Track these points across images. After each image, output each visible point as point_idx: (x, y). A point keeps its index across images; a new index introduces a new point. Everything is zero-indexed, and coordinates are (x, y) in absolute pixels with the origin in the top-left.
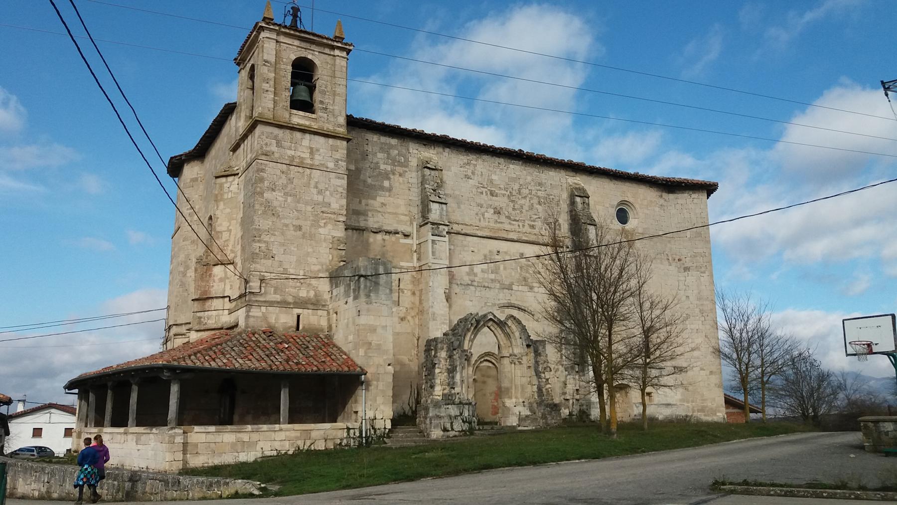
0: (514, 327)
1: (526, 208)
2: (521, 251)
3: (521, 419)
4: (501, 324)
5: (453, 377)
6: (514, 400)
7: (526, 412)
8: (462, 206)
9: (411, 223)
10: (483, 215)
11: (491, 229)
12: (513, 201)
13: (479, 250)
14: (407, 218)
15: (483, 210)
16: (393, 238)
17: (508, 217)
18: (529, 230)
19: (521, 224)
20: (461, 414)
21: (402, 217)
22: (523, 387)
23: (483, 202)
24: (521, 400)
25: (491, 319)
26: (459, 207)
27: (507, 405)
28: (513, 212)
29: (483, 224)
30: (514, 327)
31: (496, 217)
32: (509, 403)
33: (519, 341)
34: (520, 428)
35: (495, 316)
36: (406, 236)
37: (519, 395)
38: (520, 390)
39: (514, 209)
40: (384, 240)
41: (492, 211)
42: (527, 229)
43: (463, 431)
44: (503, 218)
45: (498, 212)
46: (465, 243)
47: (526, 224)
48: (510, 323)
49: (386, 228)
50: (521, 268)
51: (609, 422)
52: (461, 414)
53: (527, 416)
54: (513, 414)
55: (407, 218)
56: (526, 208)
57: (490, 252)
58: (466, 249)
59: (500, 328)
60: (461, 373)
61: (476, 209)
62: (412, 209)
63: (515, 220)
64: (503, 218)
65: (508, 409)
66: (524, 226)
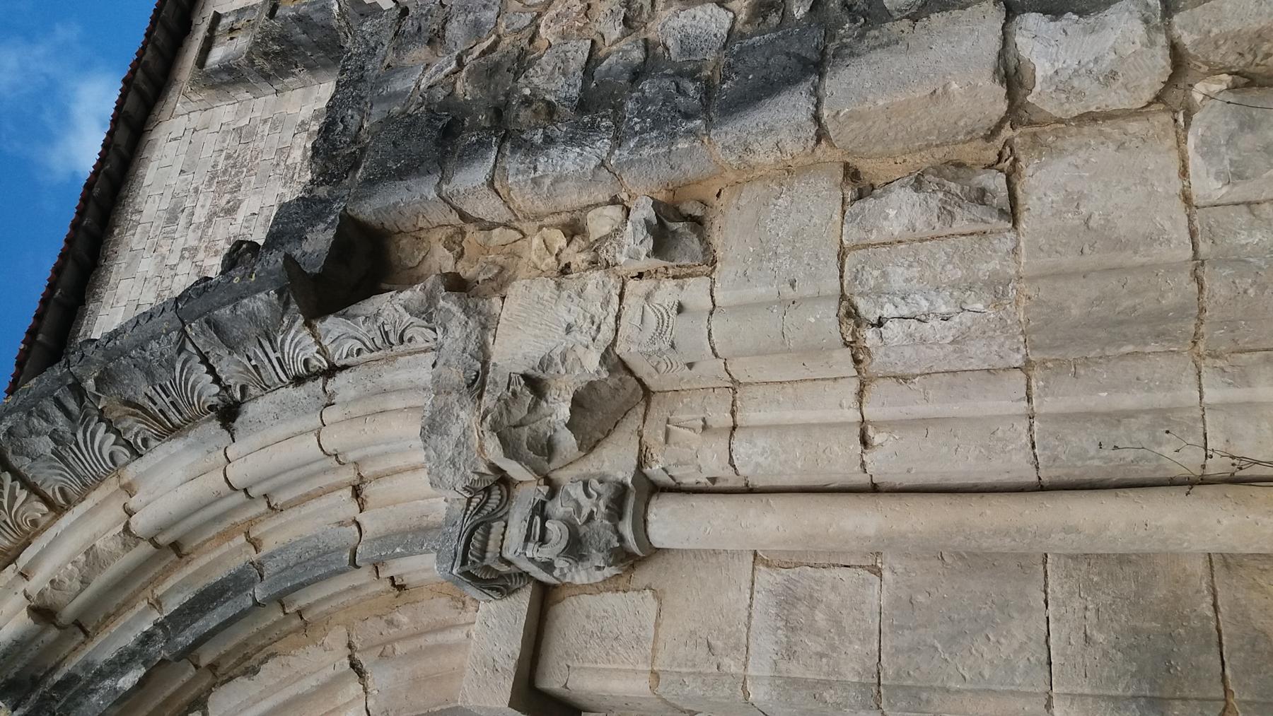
33: (276, 439)
38: (1157, 383)
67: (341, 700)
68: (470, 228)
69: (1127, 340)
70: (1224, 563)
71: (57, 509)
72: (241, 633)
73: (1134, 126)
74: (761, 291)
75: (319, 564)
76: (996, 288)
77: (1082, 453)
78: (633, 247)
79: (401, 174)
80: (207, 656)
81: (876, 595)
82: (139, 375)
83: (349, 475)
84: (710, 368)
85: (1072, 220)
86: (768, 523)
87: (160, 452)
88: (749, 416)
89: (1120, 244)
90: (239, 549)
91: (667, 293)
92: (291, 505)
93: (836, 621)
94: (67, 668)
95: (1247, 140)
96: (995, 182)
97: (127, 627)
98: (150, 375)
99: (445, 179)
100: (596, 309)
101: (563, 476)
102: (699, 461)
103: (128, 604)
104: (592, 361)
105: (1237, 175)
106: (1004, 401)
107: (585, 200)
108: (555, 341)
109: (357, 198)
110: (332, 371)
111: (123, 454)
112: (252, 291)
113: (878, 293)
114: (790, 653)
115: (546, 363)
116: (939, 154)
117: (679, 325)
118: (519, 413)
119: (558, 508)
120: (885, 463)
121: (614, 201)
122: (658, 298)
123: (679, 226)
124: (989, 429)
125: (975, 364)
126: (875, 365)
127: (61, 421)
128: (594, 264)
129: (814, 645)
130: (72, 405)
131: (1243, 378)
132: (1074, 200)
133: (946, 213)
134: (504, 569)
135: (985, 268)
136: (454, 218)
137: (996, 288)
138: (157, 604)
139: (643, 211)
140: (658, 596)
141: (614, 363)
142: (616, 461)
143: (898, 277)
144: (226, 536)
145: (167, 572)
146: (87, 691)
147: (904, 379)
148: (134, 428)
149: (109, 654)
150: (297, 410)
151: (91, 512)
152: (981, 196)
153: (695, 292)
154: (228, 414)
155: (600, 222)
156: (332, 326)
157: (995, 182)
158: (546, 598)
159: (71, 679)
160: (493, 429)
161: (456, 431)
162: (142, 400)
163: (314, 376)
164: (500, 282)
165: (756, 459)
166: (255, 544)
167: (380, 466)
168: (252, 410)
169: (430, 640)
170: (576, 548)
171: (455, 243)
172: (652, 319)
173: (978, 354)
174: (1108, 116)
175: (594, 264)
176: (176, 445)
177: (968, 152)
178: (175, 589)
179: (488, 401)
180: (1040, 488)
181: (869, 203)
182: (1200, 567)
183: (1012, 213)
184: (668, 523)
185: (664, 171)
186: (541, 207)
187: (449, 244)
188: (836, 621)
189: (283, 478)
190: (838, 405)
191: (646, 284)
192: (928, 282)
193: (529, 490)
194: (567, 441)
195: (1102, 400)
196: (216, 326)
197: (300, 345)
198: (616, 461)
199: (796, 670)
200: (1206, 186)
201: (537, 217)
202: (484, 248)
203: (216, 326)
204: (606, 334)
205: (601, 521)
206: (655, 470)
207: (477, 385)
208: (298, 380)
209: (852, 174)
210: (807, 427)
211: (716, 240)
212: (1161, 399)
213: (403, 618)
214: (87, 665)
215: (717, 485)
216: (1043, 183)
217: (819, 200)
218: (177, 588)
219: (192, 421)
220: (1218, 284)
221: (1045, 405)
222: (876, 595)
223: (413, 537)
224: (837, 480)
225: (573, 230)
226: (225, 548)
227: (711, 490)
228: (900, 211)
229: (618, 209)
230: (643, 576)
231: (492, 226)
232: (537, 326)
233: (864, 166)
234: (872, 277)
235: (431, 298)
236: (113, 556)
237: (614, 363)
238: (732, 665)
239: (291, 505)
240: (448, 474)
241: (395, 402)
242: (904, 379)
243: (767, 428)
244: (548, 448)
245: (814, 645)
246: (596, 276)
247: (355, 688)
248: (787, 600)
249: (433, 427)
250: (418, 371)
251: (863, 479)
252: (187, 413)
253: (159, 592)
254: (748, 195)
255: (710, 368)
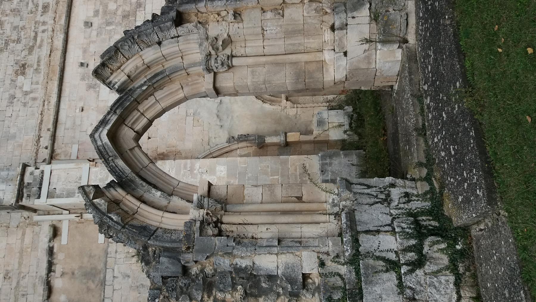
0: (130, 66)
1: (16, 21)
2: (82, 25)
3: (387, 35)
4: (128, 102)
5: (271, 278)
6: (328, 56)
7: (361, 23)
8: (12, 131)
9: (37, 224)
10: (26, 93)
11: (48, 78)
12: (7, 44)
13: (81, 99)
14: (28, 231)
15: (19, 95)
16: (59, 257)
17: (31, 50)
18: (51, 13)
19: (41, 28)
20: (393, 266)
21: (28, 240)
22: (290, 33)
23: (7, 95)
24: (328, 35)
25: (113, 136)
26: (14, 137)
27: (340, 75)
28: (24, 41)
29: (40, 94)
30: (130, 66)
31: (29, 72)
32: (335, 70)
33: (168, 48)
34: (412, 39)
35: (103, 122)
36: (56, 232)
37: (312, 43)
38: (299, 40)
39: (18, 41)
40: (63, 274)
41: (21, 78)
42: (48, 18)
43: (453, 268)
44: (32, 59)
45: (22, 69)
46: (69, 124)
47: (42, 19)
48: (119, 78)
49: (43, 272)
50: (108, 24)
51: (204, 290)
52: (393, 266)
53: (375, 17)
54: (368, 59)
55: (28, 231)
56: (16, 21)
57: (83, 79)
58: (78, 122)
59: (137, 102)
60: (254, 243)
61: (17, 106)
62: (13, 224)
63: (35, 38)
64: (32, 59)
65: (353, 73)
66: (44, 23)
67: (179, 93)
68: (199, 13)
69: (526, 295)
70: (306, 63)
71: (127, 60)
72: (161, 82)
73: (298, 5)
74: (250, 25)
75: (175, 70)
76: (281, 26)
77: (291, 48)
78: (230, 17)
79: (187, 3)
80: (155, 86)
81: (265, 70)
82: (145, 36)
83: (181, 55)
84: (242, 37)
85: (290, 18)
86: (250, 61)
87: (147, 50)
88: (248, 45)
89: (296, 21)
90: (161, 67)
91: (236, 25)
92: (170, 60)
93: (259, 74)
94: (130, 87)
95: (310, 9)
96: (281, 12)
97: (141, 81)
98: (147, 36)
99: (196, 4)
100: (225, 27)
101: (219, 54)
102: (77, 180)
103: (140, 77)
104: (225, 36)
105: (308, 13)
106: (281, 42)
107: (221, 9)
108: (219, 32)
109: (179, 7)
110: (178, 36)
111: (140, 50)
112: (167, 22)
113: (266, 26)
114: (253, 78)
115: (218, 35)
116: (274, 7)
117: (238, 30)
118: (214, 43)
119: (219, 59)
120: (267, 51)
121: (225, 10)
122: (235, 26)
123: (237, 15)
124: (280, 46)
125: (278, 37)
126: (265, 38)
127: (130, 43)
128: (223, 20)
129: (256, 77)
130: (132, 41)
131: (309, 39)
132: (291, 15)
133: (275, 16)
134: (211, 68)
135: (280, 23)
136: (197, 11)
137: (281, 26)
138: (146, 77)
139: (231, 12)
140: (233, 73)
141: (229, 36)
142: (228, 51)
143: (269, 24)
144: (158, 65)
145: (147, 71)
146: (135, 91)
147: (269, 39)
148: (142, 45)
149: (139, 84)
150: (172, 43)
151: (134, 60)
152: (279, 14)
153: (241, 25)
154: (159, 43)
155: (223, 13)
156: (179, 28)
157: (281, 12)
158: (215, 74)
159: (131, 90)
160: (211, 45)
161: (204, 46)
162: (144, 40)
163: (175, 37)
164: (207, 23)
165: (249, 51)
166: (163, 66)
167: (186, 53)
168: (164, 43)
169: (195, 82)
170: (222, 64)
171: (196, 15)
172: (234, 29)
173: (279, 35)
174: (295, 4)
175: (223, 20)
176: (150, 49)
177: (278, 7)
178: (149, 74)
179: (209, 41)
180: (285, 54)
181: (265, 13)
182: (304, 64)
183: (283, 16)
184: (235, 62)
185: (234, 6)
186: (213, 10)
187: (196, 16)
188: (259, 74)
189: (159, 59)
190: (260, 43)
191: (233, 24)
192: (273, 26)
193: (214, 57)
194: (221, 48)
195: (293, 42)
196: (160, 27)
197: (173, 32)
198: (228, 51)
199: (254, 80)
200: (305, 14)
201: (211, 12)
202: (202, 17)
203: (160, 27)
204: (227, 31)
205: (226, 60)
206: (234, 53)
207: (207, 38)
208: (172, 38)
209: (262, 9)
210: (256, 46)
211: (243, 18)
212: (299, 42)
213: (190, 79)
214: (134, 87)
215: (76, 208)
216: (287, 12)
217: (257, 13)
218: (150, 74)
219: (152, 45)
220: (305, 27)
221: (287, 43)
222: (265, 70)
223: (194, 64)
224: (260, 54)
225: (219, 14)
226: (158, 67)
227: (242, 56)
228: (269, 15)
229: (226, 12)
230: (231, 70)
231: (203, 13)
232: (215, 29)
233: (264, 8)
234: (265, 24)
235: (197, 25)
236: (140, 67)
237: (229, 36)
238: (245, 81)
239: (170, 60)
240: (203, 52)
241: (191, 41)
242: (269, 39)
243: (250, 47)
244: (218, 49)
245: (256, 77)
246: (224, 23)
247: (181, 91)
248: (253, 72)
249: (201, 45)
250: (196, 36)
251: (263, 54)
252: (152, 43)
253: (146, 74)
254: (248, 11)
255: (242, 37)
